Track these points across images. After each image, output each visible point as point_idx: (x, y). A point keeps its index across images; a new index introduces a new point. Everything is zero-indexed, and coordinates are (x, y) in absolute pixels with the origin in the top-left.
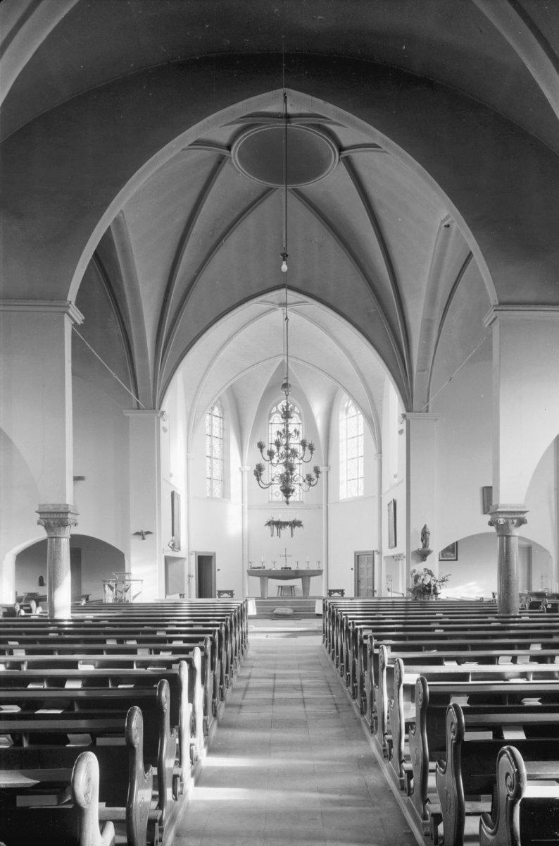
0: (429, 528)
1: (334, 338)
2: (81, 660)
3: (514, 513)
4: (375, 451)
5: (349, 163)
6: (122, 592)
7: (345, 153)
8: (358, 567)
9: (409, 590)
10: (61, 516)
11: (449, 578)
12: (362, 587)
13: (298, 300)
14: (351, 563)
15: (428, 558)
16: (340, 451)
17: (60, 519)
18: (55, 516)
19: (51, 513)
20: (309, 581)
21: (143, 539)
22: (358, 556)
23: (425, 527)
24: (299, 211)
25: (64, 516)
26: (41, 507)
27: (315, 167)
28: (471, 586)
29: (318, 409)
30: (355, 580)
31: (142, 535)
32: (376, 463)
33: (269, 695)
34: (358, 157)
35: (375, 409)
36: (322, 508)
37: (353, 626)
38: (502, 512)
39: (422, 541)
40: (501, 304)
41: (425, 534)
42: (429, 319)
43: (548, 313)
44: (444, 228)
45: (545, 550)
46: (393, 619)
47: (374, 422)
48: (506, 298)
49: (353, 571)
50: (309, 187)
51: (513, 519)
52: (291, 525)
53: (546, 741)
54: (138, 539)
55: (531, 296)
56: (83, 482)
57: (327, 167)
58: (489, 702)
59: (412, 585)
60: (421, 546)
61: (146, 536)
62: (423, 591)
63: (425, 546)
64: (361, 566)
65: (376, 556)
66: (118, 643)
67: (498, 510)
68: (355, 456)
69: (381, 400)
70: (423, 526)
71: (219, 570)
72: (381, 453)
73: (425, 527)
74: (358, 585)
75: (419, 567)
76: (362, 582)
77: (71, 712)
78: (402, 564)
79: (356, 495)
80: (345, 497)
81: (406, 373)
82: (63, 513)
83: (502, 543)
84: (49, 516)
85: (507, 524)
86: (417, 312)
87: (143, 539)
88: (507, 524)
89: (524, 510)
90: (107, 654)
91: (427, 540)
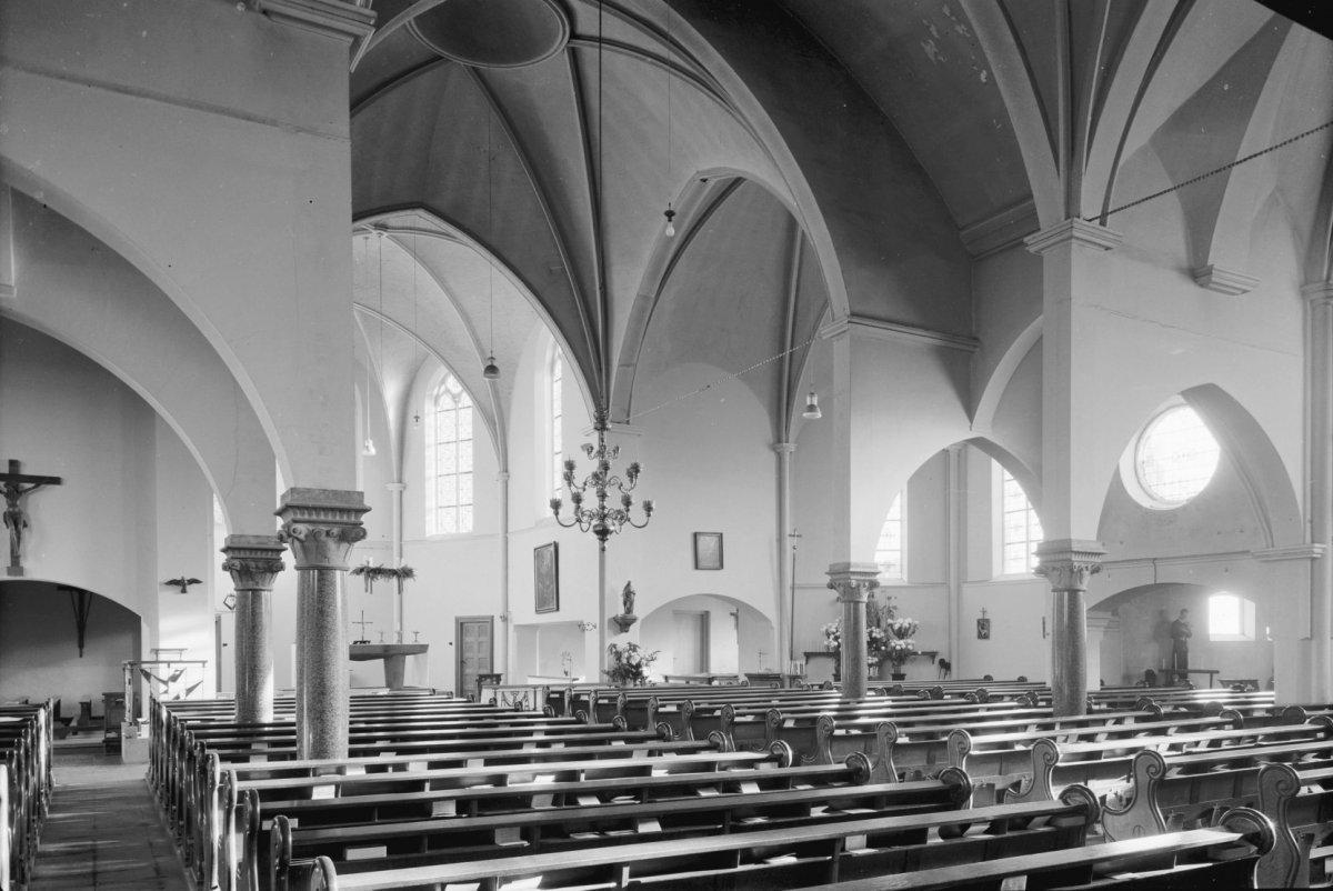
0: (634, 587)
1: (447, 290)
2: (583, 771)
3: (866, 573)
4: (496, 468)
5: (574, 55)
6: (165, 683)
7: (577, 43)
8: (462, 640)
9: (603, 672)
10: (270, 555)
11: (659, 655)
12: (468, 671)
13: (434, 228)
14: (452, 636)
15: (632, 627)
16: (427, 462)
17: (267, 561)
18: (259, 555)
19: (251, 550)
20: (404, 661)
21: (184, 591)
22: (462, 624)
23: (629, 585)
24: (473, 101)
25: (274, 557)
26: (236, 540)
27: (524, 47)
28: (667, 663)
29: (391, 391)
30: (457, 662)
31: (181, 584)
32: (499, 487)
33: (105, 865)
34: (589, 52)
35: (499, 406)
36: (392, 548)
37: (203, 750)
38: (854, 573)
39: (625, 604)
40: (853, 314)
41: (628, 595)
42: (645, 297)
43: (870, 329)
44: (698, 182)
45: (765, 619)
46: (471, 719)
47: (496, 420)
48: (858, 308)
49: (453, 647)
50: (501, 72)
51: (864, 580)
52: (399, 577)
53: (716, 876)
54: (174, 592)
55: (881, 309)
56: (57, 487)
57: (544, 50)
58: (898, 804)
59: (609, 662)
60: (621, 611)
61: (188, 588)
62: (627, 671)
63: (629, 611)
64: (468, 639)
65: (498, 625)
66: (566, 746)
67: (851, 570)
68: (453, 470)
69: (510, 394)
70: (625, 585)
71: (225, 645)
72: (507, 471)
73: (629, 585)
74: (462, 667)
75: (622, 641)
76: (469, 663)
77: (419, 855)
78: (592, 637)
79: (454, 531)
80: (434, 533)
81: (600, 364)
82: (272, 550)
83: (848, 610)
84: (248, 554)
85: (858, 586)
86: (628, 284)
87: (184, 591)
88: (858, 586)
89: (873, 571)
90: (394, 770)
91: (631, 604)
